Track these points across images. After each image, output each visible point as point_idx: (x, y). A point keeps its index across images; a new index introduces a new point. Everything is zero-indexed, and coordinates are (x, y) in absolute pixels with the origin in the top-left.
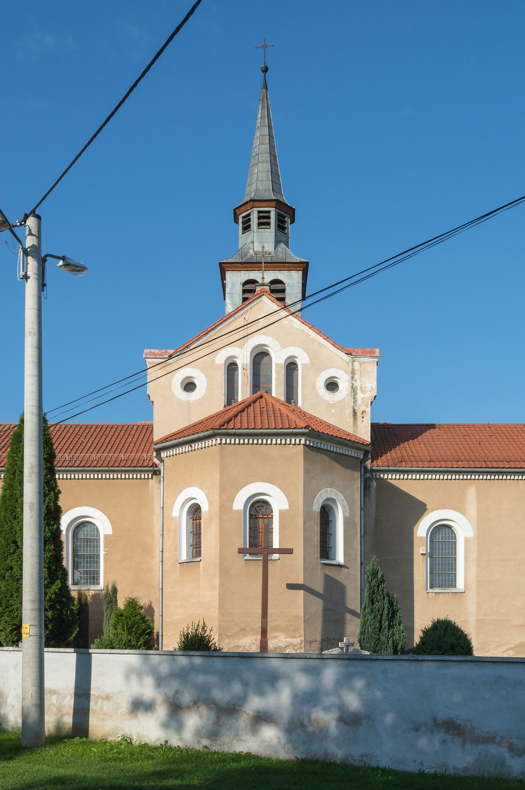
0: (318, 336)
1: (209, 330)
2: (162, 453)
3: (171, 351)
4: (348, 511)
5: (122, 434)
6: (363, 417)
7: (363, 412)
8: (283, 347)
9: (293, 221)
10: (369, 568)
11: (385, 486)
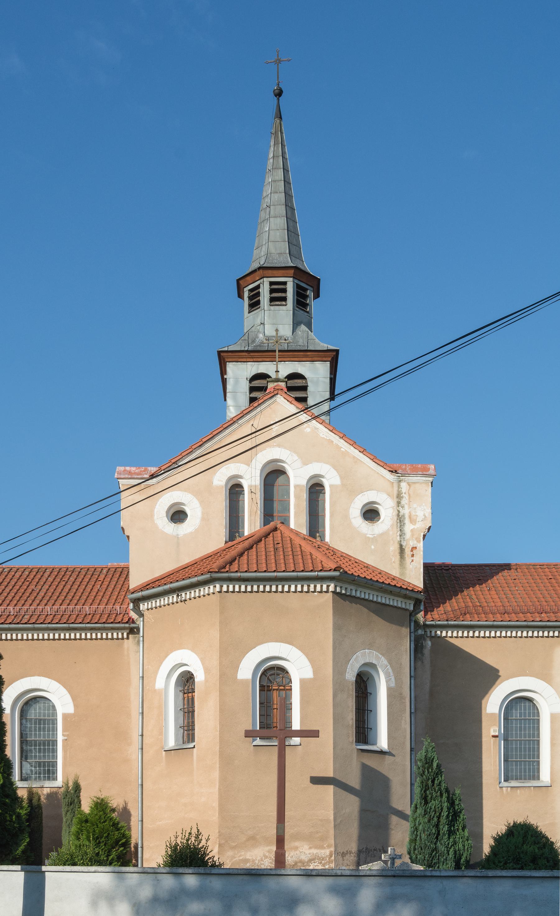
0: (352, 448)
2: (141, 605)
3: (153, 470)
5: (86, 580)
6: (413, 556)
7: (414, 548)
8: (305, 463)
9: (317, 295)
10: (421, 754)
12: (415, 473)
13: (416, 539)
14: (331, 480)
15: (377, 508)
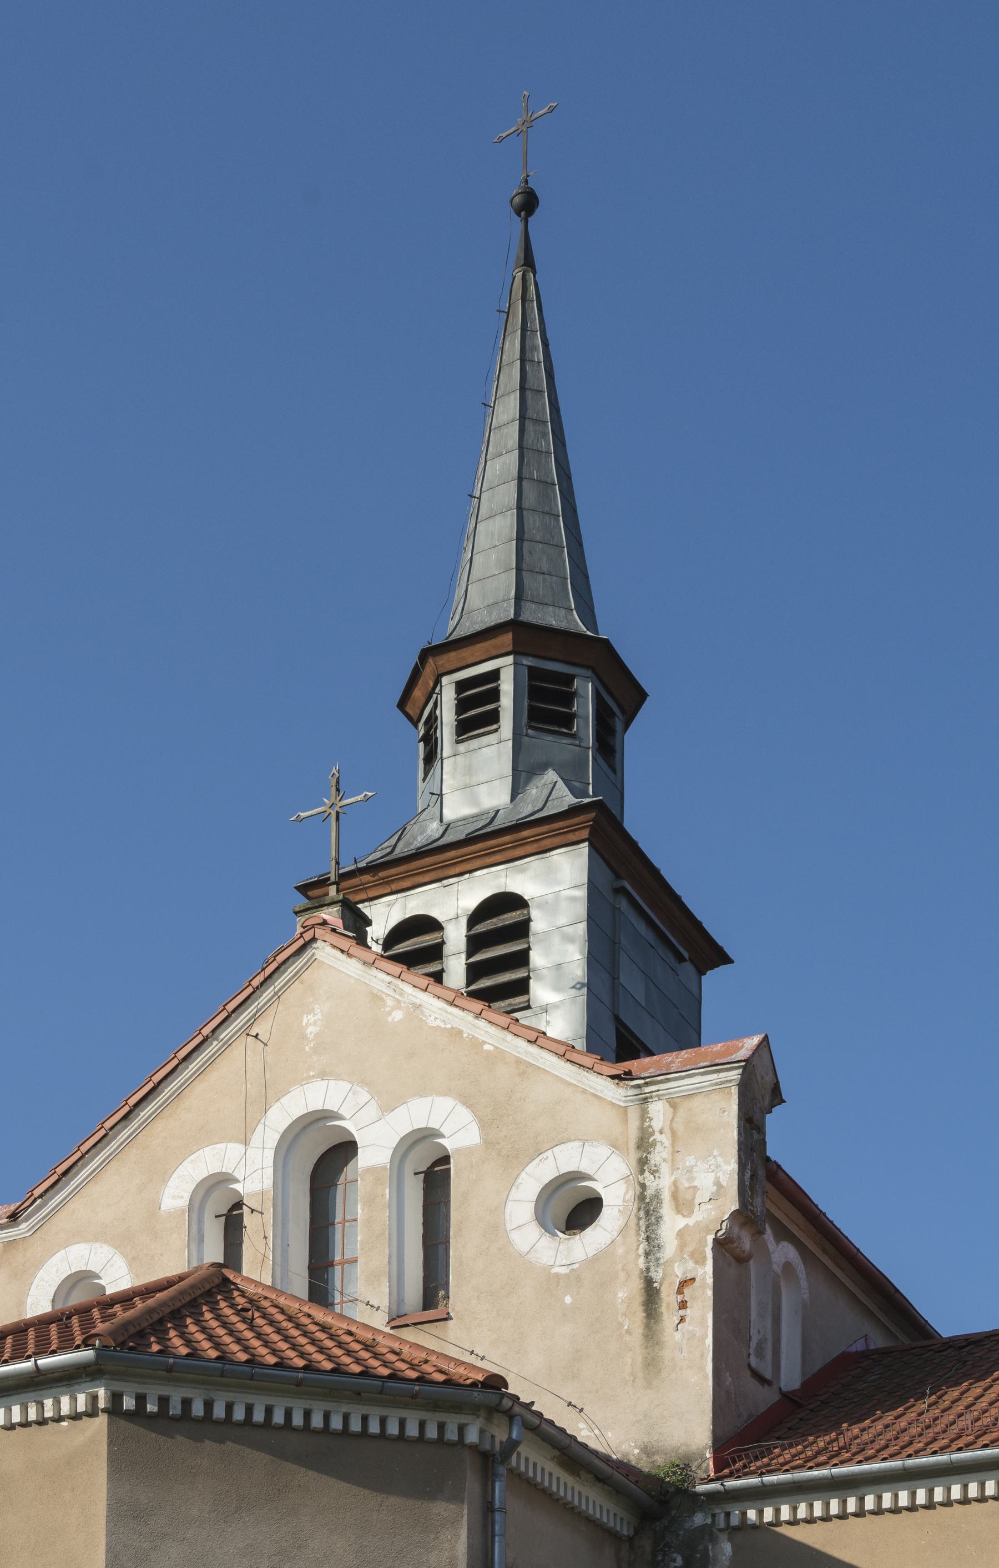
0: (510, 1037)
1: (132, 1101)
6: (683, 1305)
7: (686, 1283)
8: (387, 1108)
13: (692, 1255)
14: (460, 1133)
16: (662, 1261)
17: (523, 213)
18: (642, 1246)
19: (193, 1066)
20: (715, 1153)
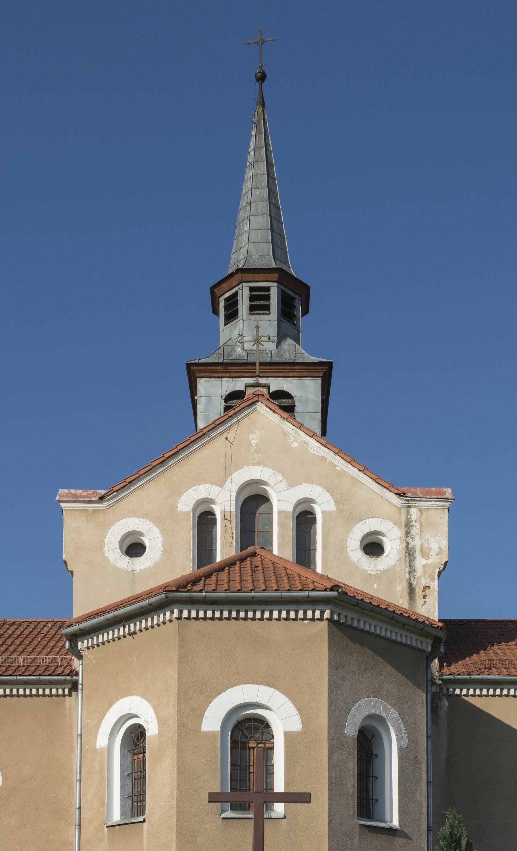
0: (350, 466)
1: (167, 456)
2: (80, 644)
3: (103, 492)
4: (406, 738)
5: (26, 633)
6: (425, 597)
7: (426, 588)
8: (292, 484)
9: (306, 311)
10: (445, 830)
11: (461, 707)
12: (428, 497)
14: (323, 505)
15: (381, 540)
16: (416, 577)
17: (260, 81)
18: (407, 569)
19: (196, 446)
20: (439, 535)
